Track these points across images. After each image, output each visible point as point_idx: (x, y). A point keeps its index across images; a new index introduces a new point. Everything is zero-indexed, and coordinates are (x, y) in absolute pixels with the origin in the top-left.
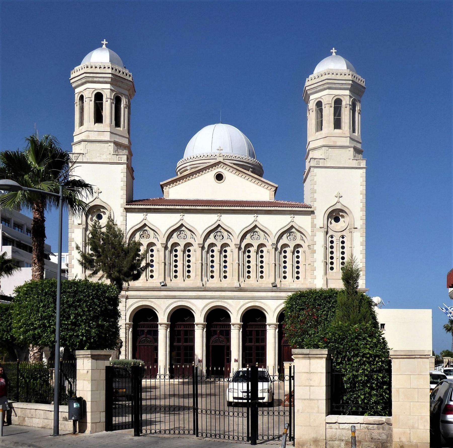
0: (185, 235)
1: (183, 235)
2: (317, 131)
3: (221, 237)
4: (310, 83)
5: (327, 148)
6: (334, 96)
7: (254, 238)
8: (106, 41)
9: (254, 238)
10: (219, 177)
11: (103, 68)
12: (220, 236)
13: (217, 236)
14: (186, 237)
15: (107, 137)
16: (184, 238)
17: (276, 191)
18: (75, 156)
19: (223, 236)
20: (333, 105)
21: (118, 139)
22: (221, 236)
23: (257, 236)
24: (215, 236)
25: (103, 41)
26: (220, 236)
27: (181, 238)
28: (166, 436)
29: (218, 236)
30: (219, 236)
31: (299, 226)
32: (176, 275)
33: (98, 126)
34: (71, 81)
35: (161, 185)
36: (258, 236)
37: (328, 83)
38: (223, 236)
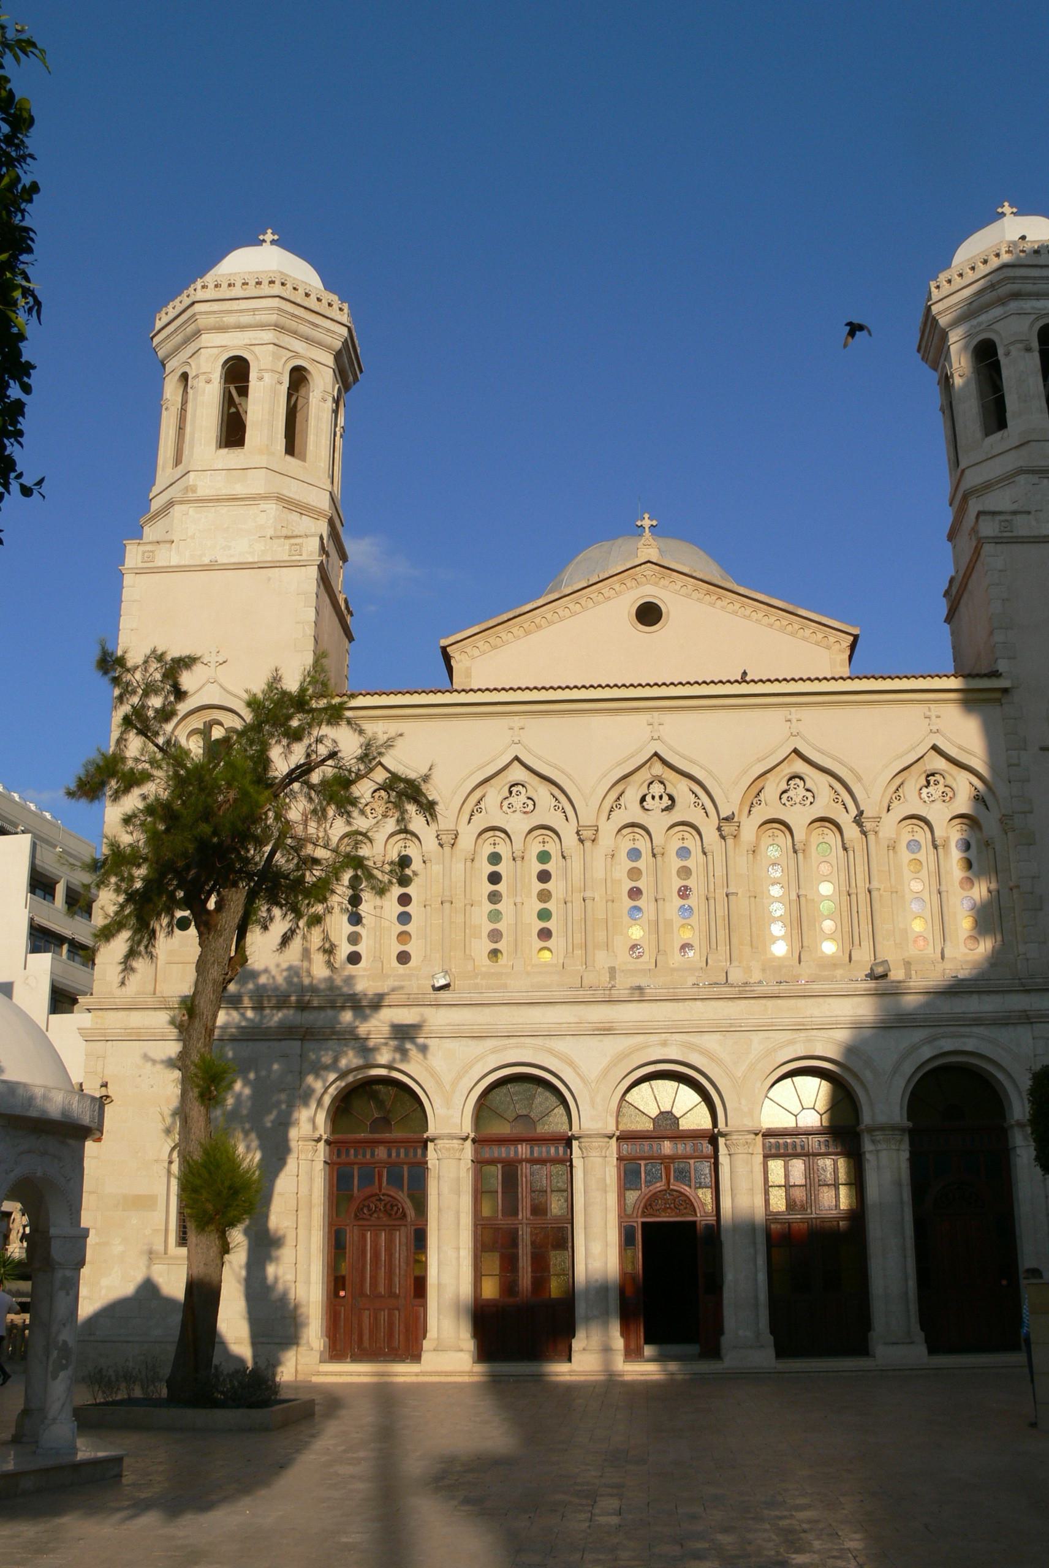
0: (529, 798)
1: (522, 798)
2: (988, 433)
3: (666, 801)
4: (946, 289)
5: (1034, 479)
6: (1034, 316)
7: (789, 799)
8: (273, 234)
9: (789, 799)
10: (649, 614)
11: (254, 283)
12: (661, 797)
13: (648, 798)
14: (531, 807)
15: (257, 483)
16: (525, 810)
17: (853, 647)
18: (144, 552)
19: (671, 798)
20: (1035, 345)
21: (294, 491)
22: (666, 798)
23: (801, 791)
24: (643, 799)
25: (265, 233)
26: (661, 797)
27: (512, 810)
28: (726, 1171)
29: (653, 797)
30: (657, 798)
31: (960, 748)
32: (497, 930)
33: (231, 457)
34: (156, 340)
35: (444, 650)
36: (808, 790)
37: (1008, 278)
38: (671, 798)
